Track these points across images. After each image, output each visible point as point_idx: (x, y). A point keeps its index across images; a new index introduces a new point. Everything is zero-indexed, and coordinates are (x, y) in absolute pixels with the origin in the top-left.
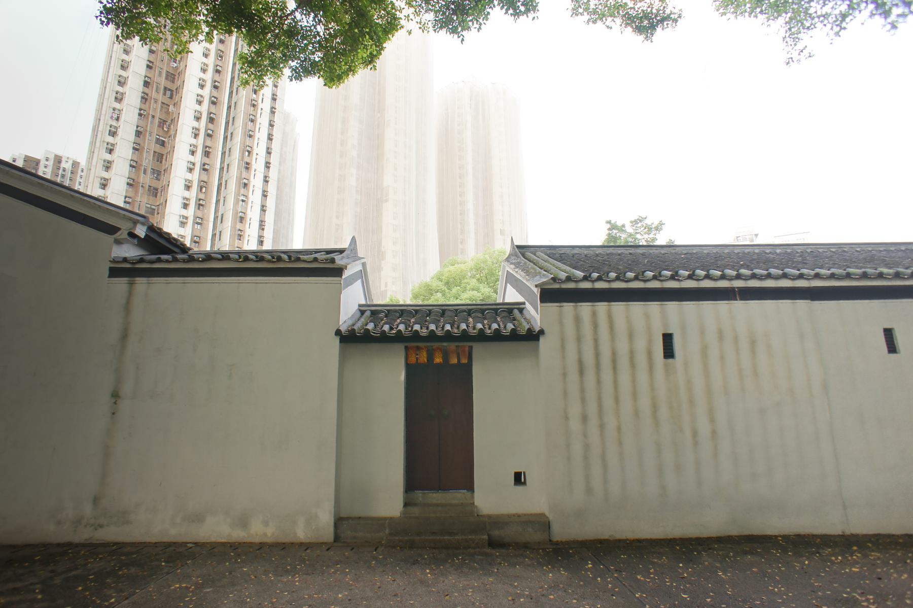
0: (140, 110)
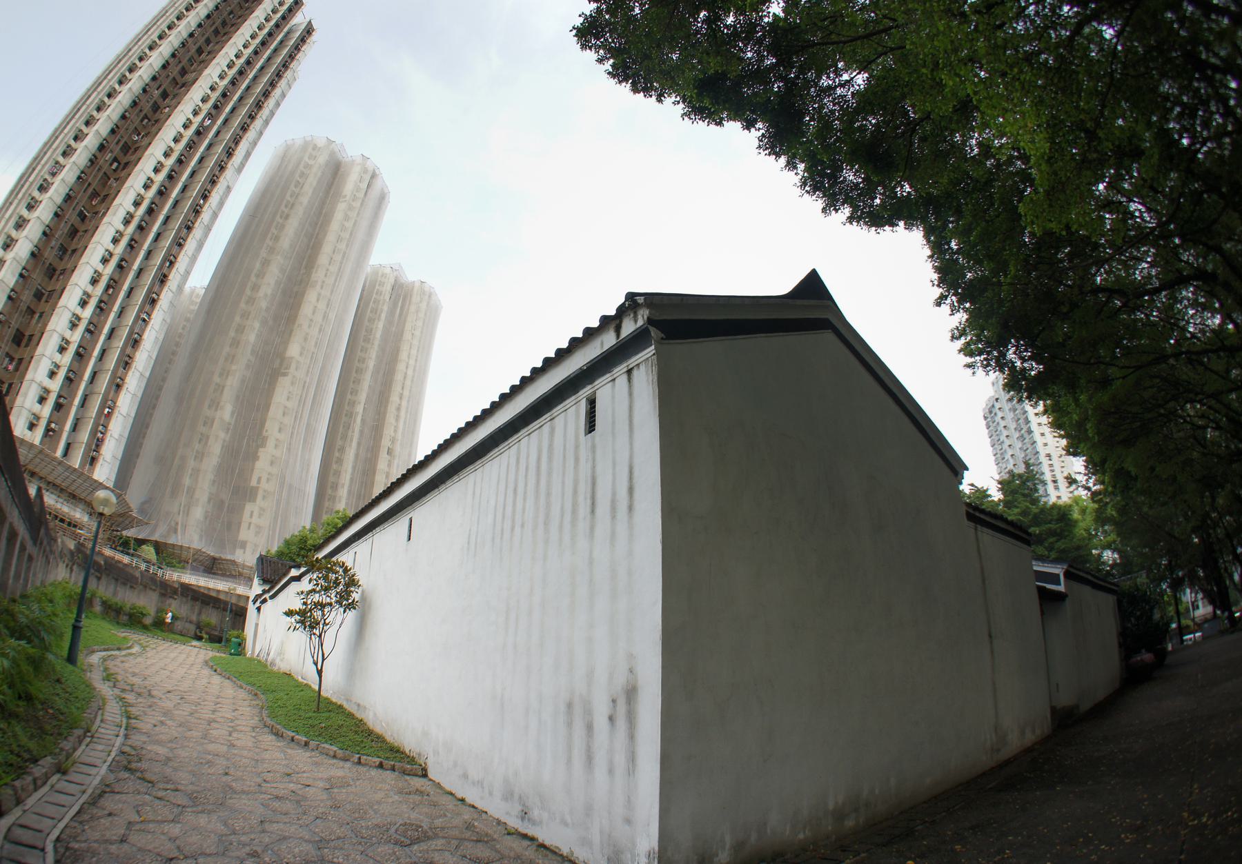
0: (82, 172)
